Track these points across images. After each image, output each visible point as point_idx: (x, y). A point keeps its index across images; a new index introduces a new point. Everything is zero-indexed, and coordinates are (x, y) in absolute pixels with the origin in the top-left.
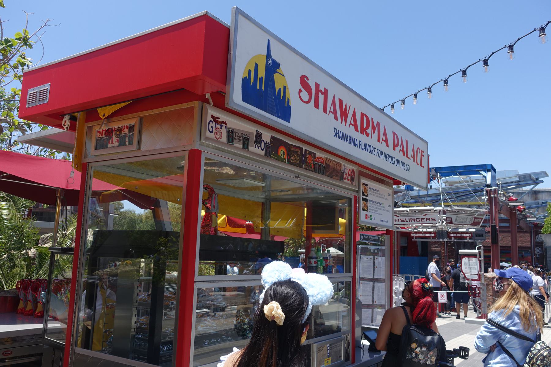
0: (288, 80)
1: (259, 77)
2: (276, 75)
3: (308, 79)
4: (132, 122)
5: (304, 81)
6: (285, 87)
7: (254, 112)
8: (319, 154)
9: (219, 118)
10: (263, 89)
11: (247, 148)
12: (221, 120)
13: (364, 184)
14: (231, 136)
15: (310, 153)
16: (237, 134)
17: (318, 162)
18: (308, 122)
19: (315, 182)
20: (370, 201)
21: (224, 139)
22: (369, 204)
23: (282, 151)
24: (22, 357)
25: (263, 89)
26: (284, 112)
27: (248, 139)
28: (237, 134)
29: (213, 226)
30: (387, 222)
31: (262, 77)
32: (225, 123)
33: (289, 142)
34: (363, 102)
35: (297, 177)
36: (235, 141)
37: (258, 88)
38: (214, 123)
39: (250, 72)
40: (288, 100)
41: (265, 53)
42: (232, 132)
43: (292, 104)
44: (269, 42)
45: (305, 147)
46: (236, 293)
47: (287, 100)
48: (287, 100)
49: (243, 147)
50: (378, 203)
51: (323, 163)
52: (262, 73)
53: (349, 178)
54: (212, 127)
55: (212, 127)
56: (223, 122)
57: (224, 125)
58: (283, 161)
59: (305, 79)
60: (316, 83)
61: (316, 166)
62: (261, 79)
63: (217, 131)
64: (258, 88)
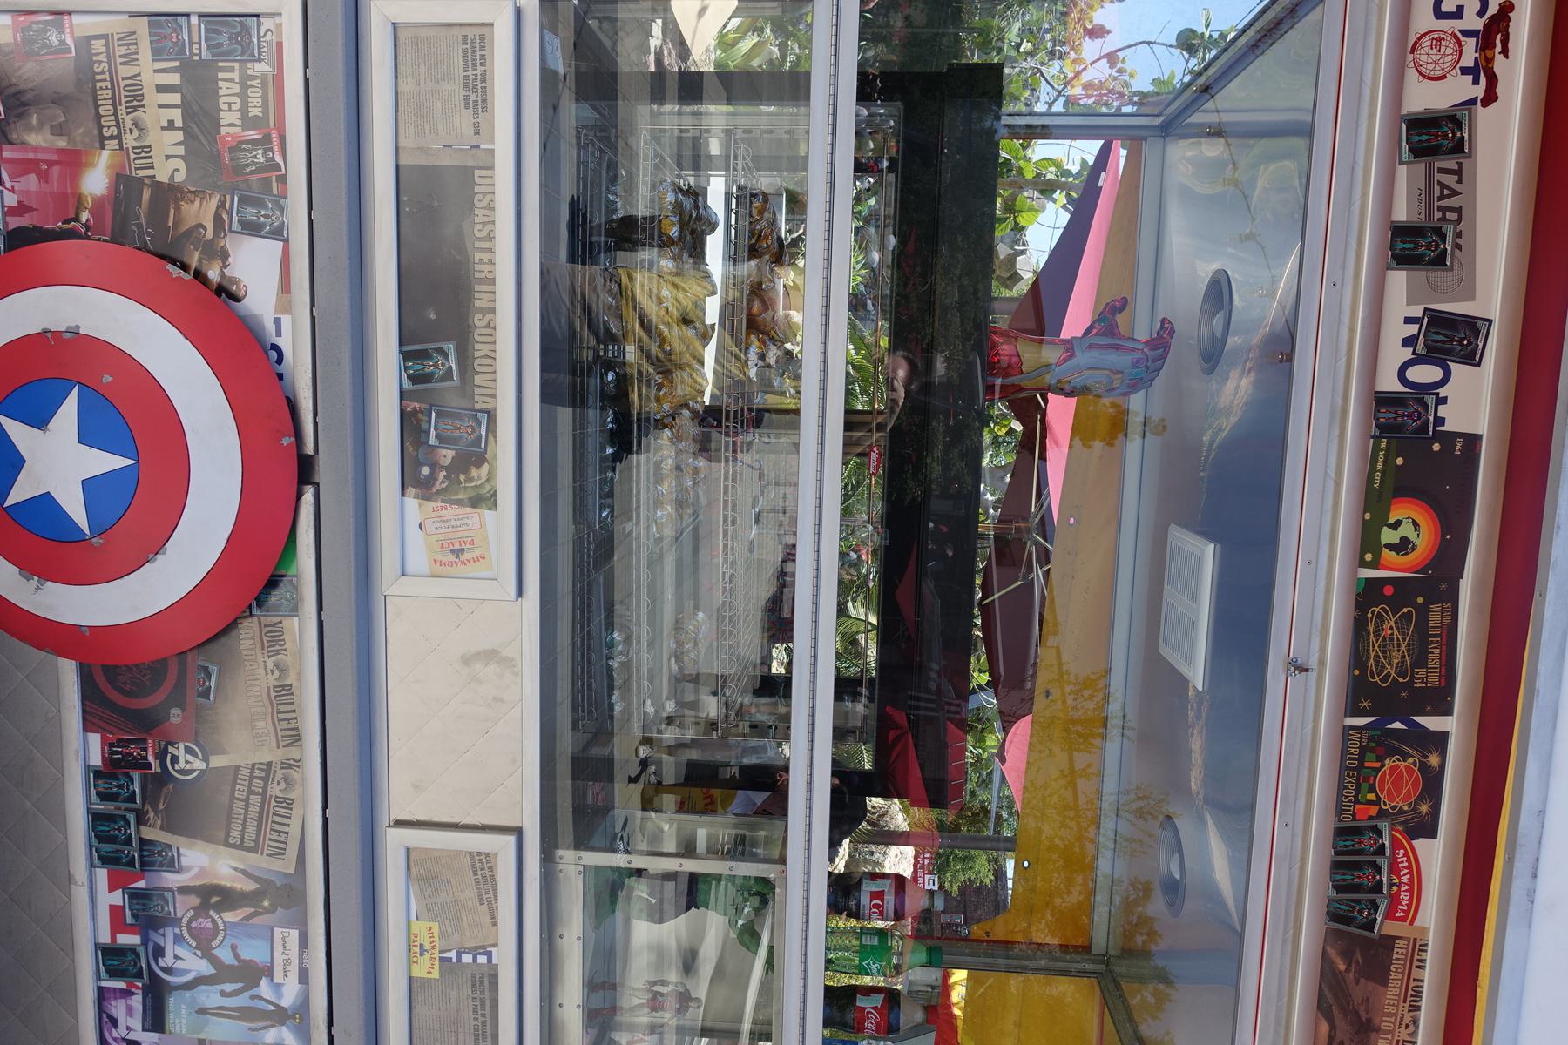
8: (1436, 858)
9: (1505, 52)
11: (1403, 260)
12: (1499, 64)
13: (1440, 183)
14: (1435, 139)
15: (1432, 783)
16: (1450, 180)
21: (1425, 97)
23: (1412, 525)
24: (1344, 267)
27: (1440, 261)
28: (1450, 180)
32: (1490, 98)
33: (1466, 586)
36: (1420, 168)
38: (1478, 24)
42: (1458, 148)
45: (1455, 726)
46: (48, 18)
51: (1390, 916)
56: (1492, 80)
57: (1479, 91)
58: (1367, 544)
60: (1109, 32)
61: (1367, 842)
63: (1449, 48)
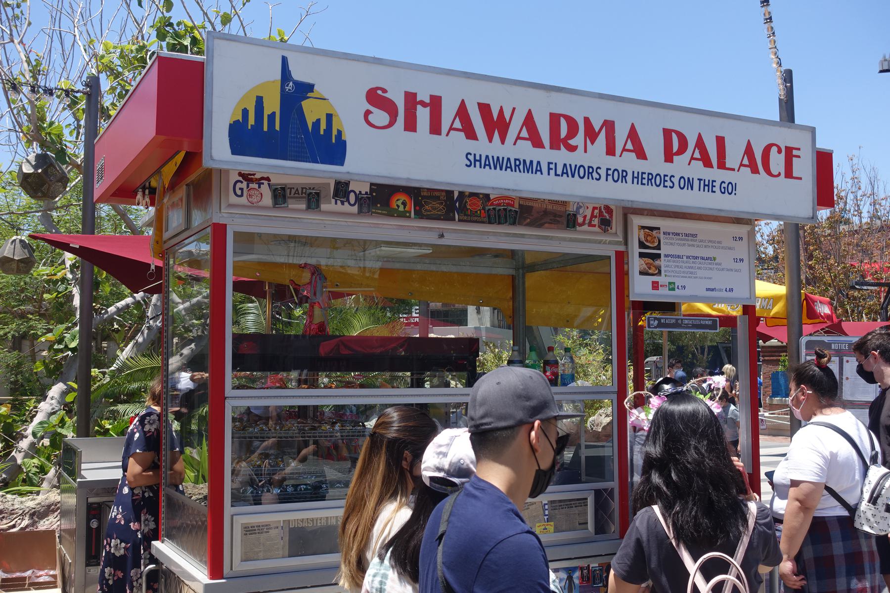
0: (340, 100)
1: (267, 112)
2: (305, 104)
3: (385, 91)
4: (180, 196)
5: (376, 98)
6: (329, 117)
7: (260, 165)
9: (254, 175)
10: (277, 128)
12: (258, 176)
17: (499, 205)
18: (376, 154)
19: (492, 238)
20: (666, 256)
22: (662, 262)
25: (277, 128)
26: (332, 149)
29: (171, 314)
30: (731, 290)
31: (274, 113)
34: (554, 94)
35: (442, 236)
37: (265, 129)
38: (245, 183)
39: (245, 112)
40: (340, 133)
41: (278, 76)
42: (283, 189)
43: (347, 136)
44: (284, 60)
47: (335, 133)
48: (335, 133)
49: (309, 207)
50: (696, 258)
51: (513, 206)
52: (272, 105)
53: (596, 221)
54: (242, 189)
55: (242, 189)
56: (263, 178)
57: (266, 182)
59: (379, 92)
61: (492, 213)
62: (272, 116)
63: (252, 192)
64: (265, 129)
